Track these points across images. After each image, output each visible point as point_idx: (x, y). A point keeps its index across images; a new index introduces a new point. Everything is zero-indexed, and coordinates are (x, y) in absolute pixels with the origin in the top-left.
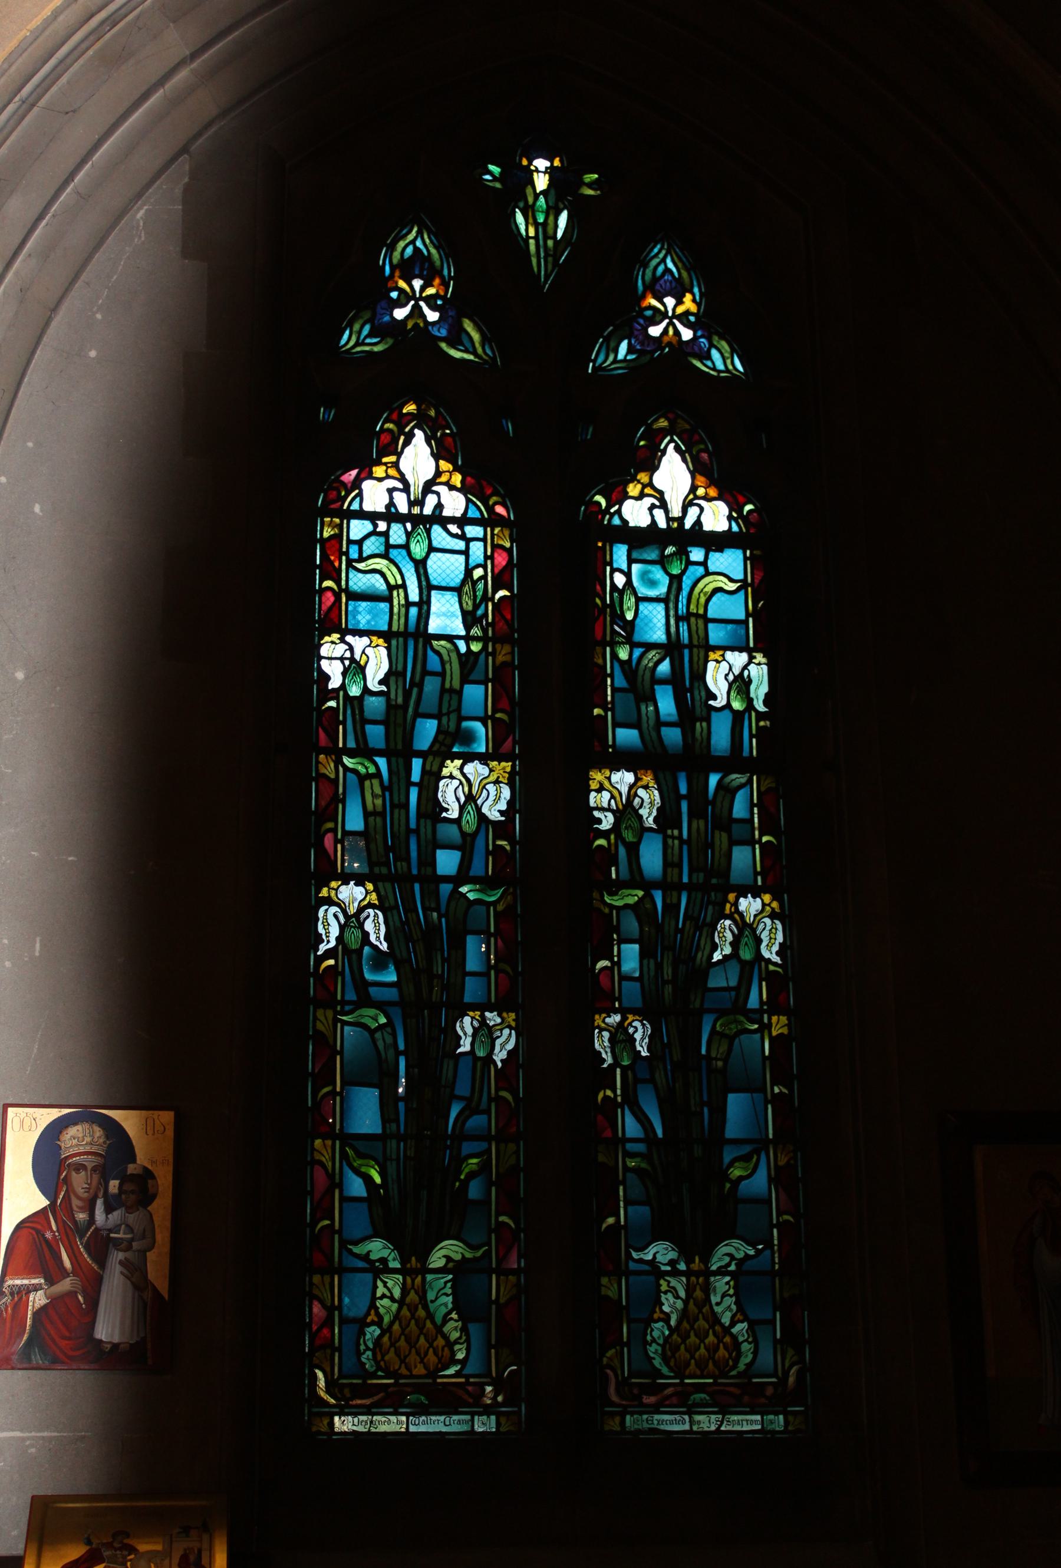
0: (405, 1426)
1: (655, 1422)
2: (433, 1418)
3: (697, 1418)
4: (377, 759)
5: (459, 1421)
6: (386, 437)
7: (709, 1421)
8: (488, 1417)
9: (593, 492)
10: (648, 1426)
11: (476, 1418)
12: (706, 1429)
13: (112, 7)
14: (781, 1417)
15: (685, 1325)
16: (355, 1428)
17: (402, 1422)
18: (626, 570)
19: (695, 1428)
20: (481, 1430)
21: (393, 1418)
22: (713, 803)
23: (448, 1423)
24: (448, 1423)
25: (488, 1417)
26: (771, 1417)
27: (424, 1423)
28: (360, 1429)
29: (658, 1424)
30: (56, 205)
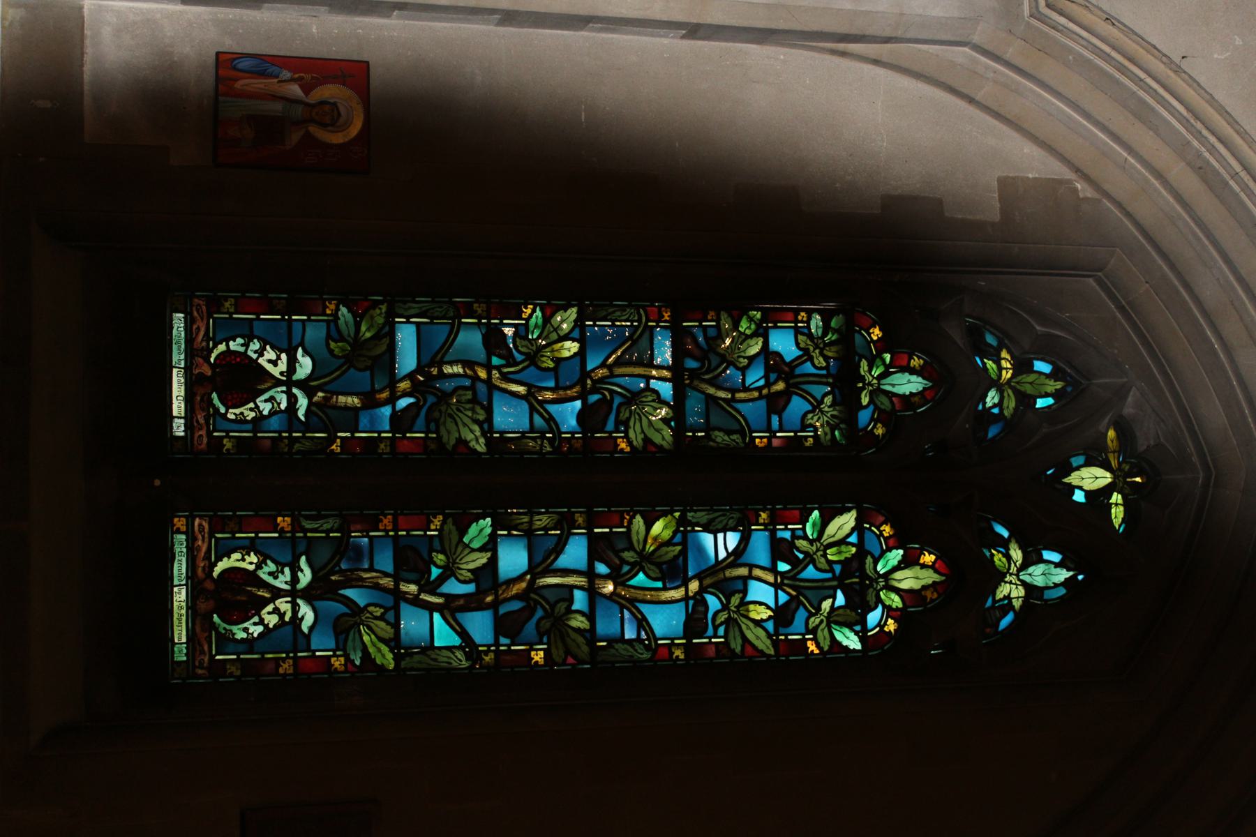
0: (177, 365)
1: (180, 558)
2: (183, 388)
4: (589, 368)
5: (181, 407)
6: (441, 560)
7: (180, 601)
8: (184, 431)
10: (177, 553)
12: (175, 599)
13: (1251, 184)
14: (185, 658)
17: (179, 363)
18: (746, 644)
19: (175, 589)
21: (182, 357)
24: (179, 398)
25: (184, 431)
26: (185, 651)
27: (179, 381)
28: (175, 332)
29: (179, 560)
30: (1103, 136)
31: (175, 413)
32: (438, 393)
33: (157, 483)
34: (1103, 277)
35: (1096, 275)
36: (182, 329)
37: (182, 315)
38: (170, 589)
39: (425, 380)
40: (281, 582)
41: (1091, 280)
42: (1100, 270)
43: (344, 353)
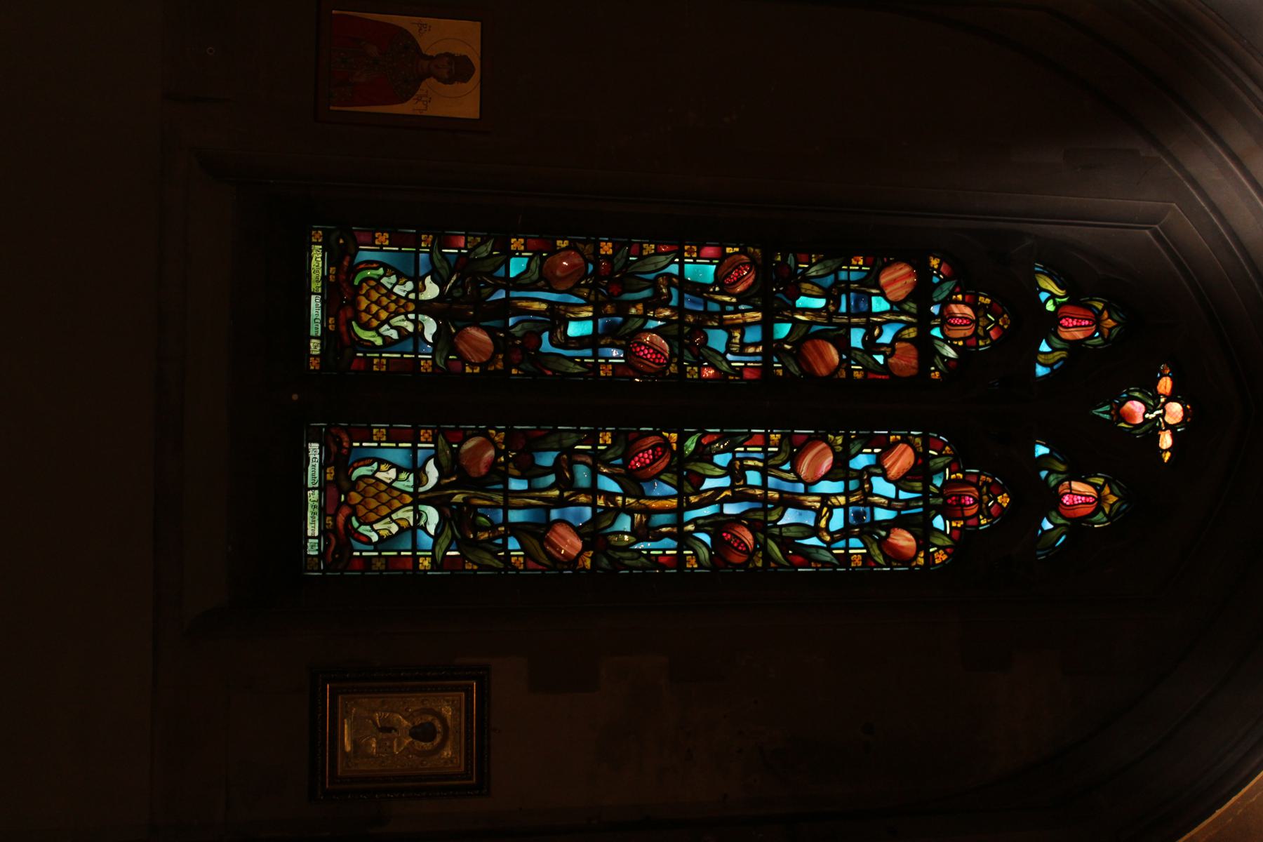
3: (317, 492)
8: (317, 550)
9: (985, 527)
10: (311, 459)
11: (317, 541)
12: (309, 499)
15: (394, 297)
16: (314, 259)
20: (311, 344)
21: (320, 284)
22: (899, 510)
23: (316, 321)
24: (316, 321)
25: (317, 550)
27: (317, 305)
28: (314, 262)
29: (313, 466)
31: (313, 333)
32: (572, 316)
33: (295, 397)
34: (1159, 229)
35: (1151, 228)
36: (320, 259)
37: (321, 247)
38: (326, 291)
39: (734, 375)
40: (406, 483)
41: (1147, 232)
42: (1155, 223)
43: (650, 344)
